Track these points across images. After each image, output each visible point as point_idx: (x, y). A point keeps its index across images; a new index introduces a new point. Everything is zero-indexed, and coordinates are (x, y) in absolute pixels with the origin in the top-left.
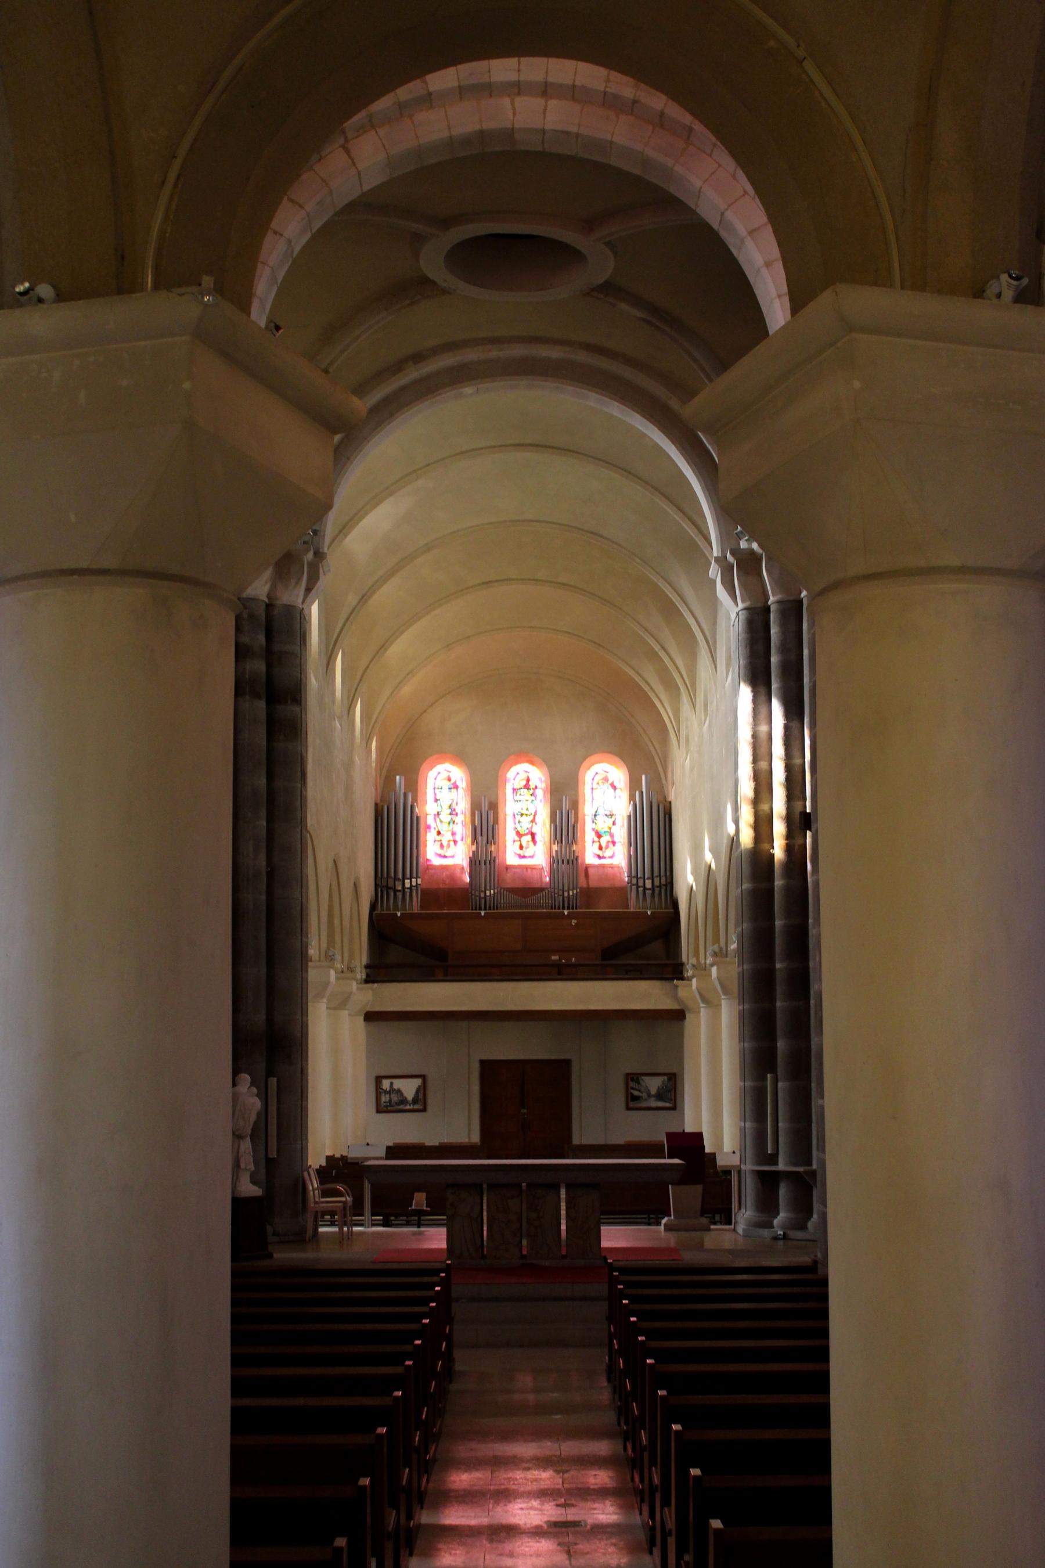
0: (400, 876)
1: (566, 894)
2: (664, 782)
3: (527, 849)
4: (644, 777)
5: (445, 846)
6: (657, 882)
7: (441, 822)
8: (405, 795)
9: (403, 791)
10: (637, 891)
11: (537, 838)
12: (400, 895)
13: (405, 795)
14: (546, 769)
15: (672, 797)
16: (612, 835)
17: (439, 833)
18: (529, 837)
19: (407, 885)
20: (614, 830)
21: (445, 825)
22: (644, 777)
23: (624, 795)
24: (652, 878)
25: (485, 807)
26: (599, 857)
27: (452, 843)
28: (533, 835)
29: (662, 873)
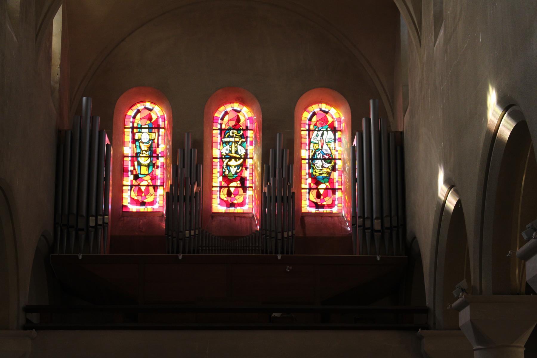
0: (84, 213)
1: (279, 236)
2: (391, 119)
3: (234, 189)
4: (371, 102)
5: (143, 190)
6: (387, 224)
7: (140, 164)
8: (93, 119)
9: (90, 113)
10: (364, 233)
11: (248, 184)
12: (83, 235)
13: (93, 119)
14: (257, 105)
15: (404, 123)
16: (331, 181)
17: (136, 177)
18: (237, 184)
19: (92, 223)
20: (335, 175)
21: (144, 170)
22: (371, 102)
23: (345, 137)
24: (381, 217)
25: (188, 145)
26: (317, 206)
27: (151, 188)
28: (243, 180)
29: (393, 213)
